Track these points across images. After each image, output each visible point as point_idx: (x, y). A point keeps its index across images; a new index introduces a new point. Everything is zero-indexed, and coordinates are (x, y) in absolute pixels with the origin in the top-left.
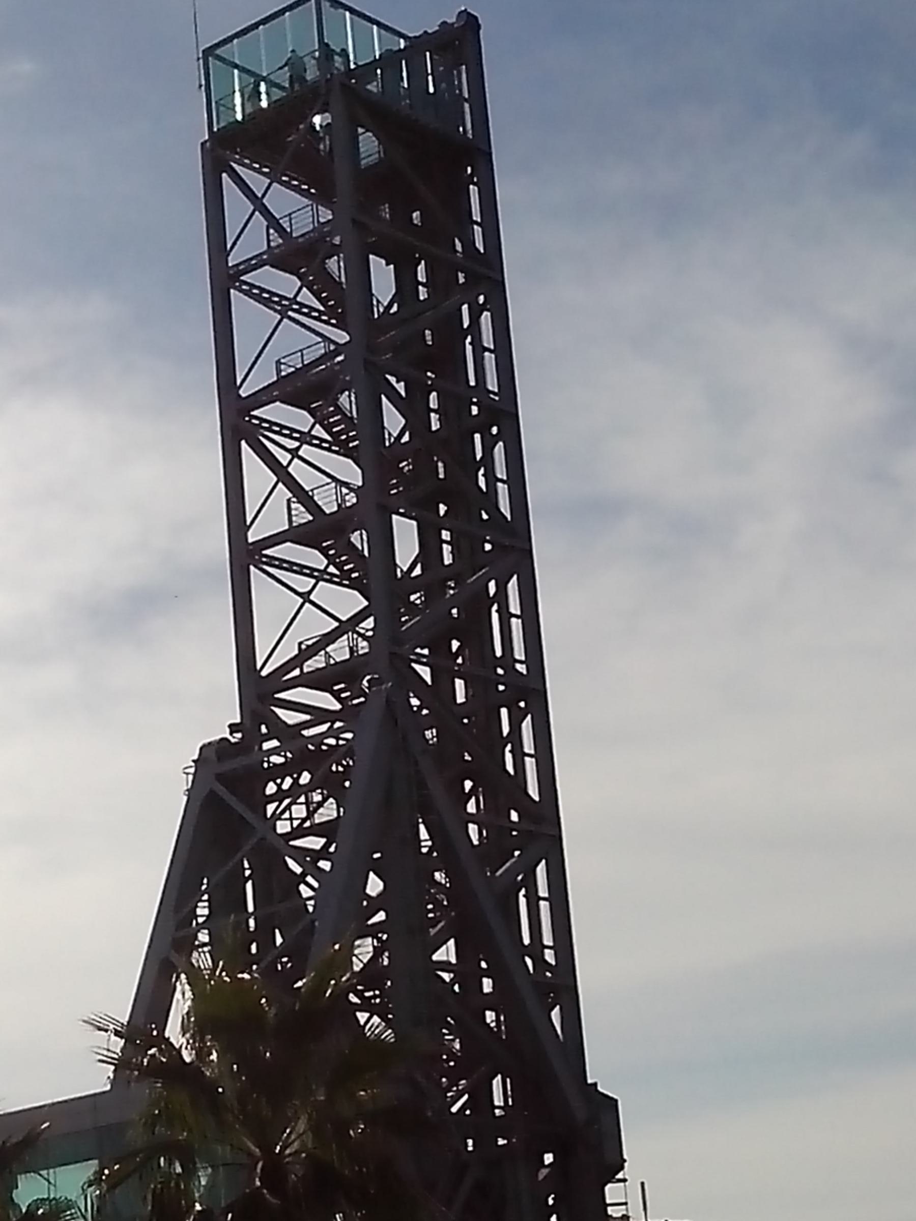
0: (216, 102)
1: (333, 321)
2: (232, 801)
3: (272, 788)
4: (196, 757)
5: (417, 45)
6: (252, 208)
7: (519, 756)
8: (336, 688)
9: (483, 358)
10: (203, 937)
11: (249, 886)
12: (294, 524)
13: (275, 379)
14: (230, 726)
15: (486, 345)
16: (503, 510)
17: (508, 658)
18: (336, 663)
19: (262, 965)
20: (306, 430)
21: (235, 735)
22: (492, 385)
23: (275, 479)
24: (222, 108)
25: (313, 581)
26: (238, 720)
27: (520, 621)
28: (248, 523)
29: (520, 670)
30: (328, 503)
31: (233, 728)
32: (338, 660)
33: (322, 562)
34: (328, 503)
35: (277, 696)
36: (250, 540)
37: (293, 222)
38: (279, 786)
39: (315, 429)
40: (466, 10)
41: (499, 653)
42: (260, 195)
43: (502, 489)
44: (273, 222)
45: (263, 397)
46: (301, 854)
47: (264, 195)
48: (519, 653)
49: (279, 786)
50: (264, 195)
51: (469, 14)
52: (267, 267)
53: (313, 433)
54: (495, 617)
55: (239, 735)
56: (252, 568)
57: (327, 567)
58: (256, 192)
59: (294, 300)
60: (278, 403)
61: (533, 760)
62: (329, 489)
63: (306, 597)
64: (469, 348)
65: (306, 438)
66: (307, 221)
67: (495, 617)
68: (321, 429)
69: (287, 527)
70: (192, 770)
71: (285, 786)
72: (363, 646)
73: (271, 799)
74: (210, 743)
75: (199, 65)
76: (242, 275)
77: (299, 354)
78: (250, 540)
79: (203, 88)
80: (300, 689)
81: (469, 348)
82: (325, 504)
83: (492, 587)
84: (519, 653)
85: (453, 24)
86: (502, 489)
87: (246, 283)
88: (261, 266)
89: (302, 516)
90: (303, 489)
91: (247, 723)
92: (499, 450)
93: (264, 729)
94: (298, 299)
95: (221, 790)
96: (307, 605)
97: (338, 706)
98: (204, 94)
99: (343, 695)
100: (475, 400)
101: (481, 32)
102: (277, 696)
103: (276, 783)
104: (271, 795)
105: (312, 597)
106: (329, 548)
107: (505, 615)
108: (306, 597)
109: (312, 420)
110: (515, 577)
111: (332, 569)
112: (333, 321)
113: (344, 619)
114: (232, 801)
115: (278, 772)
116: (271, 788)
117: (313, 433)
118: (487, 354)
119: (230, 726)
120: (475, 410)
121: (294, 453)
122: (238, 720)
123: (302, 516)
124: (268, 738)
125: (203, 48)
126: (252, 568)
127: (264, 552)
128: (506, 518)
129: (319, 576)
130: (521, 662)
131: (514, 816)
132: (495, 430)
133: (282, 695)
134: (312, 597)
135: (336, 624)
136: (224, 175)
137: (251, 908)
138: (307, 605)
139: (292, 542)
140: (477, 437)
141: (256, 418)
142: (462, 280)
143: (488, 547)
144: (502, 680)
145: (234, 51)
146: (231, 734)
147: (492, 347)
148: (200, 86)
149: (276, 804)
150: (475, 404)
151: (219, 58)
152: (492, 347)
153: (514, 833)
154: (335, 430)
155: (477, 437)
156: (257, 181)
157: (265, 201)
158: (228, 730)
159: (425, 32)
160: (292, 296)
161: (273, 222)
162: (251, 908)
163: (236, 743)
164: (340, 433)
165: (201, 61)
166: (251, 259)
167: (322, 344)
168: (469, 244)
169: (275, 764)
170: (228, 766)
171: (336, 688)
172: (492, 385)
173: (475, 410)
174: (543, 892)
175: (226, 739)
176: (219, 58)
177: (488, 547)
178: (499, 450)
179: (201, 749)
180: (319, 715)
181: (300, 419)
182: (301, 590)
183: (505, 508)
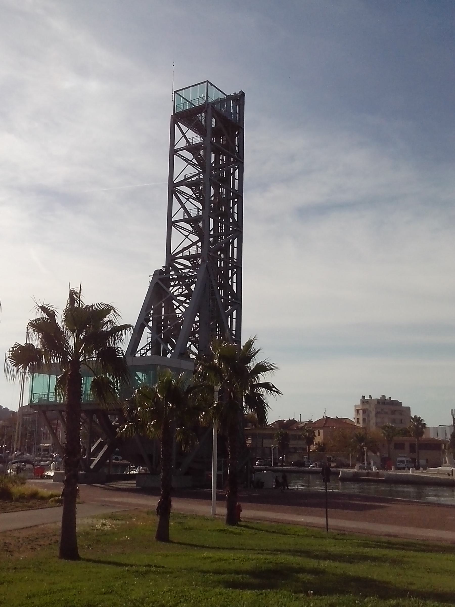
0: (176, 105)
1: (200, 167)
2: (162, 285)
3: (173, 283)
4: (153, 273)
5: (229, 98)
6: (181, 207)
7: (232, 282)
8: (190, 260)
9: (235, 181)
10: (151, 318)
11: (163, 309)
12: (185, 218)
13: (184, 179)
14: (163, 266)
15: (236, 178)
16: (235, 218)
17: (231, 329)
18: (192, 255)
19: (164, 331)
20: (191, 234)
21: (164, 269)
22: (236, 188)
23: (182, 136)
24: (177, 107)
25: (189, 233)
26: (165, 265)
27: (237, 214)
28: (175, 145)
29: (234, 333)
30: (194, 214)
31: (164, 267)
32: (192, 254)
33: (191, 193)
34: (194, 214)
35: (175, 260)
36: (173, 220)
37: (193, 140)
38: (175, 283)
39: (193, 160)
40: (242, 91)
41: (230, 256)
42: (185, 133)
43: (235, 285)
44: (186, 210)
45: (181, 183)
46: (179, 301)
47: (185, 203)
48: (235, 257)
49: (175, 283)
50: (185, 203)
51: (243, 92)
52: (185, 150)
53: (193, 196)
54: (231, 247)
55: (165, 269)
56: (172, 227)
57: (193, 194)
58: (184, 131)
59: (191, 161)
60: (184, 186)
61: (236, 249)
62: (195, 210)
63: (187, 236)
64: (232, 178)
65: (191, 197)
66: (194, 250)
67: (231, 247)
68: (195, 160)
69: (183, 218)
70: (152, 276)
71: (176, 283)
72: (199, 251)
73: (171, 286)
74: (158, 270)
75: (173, 95)
76: (178, 151)
77: (192, 139)
78: (173, 220)
79: (173, 101)
80: (182, 259)
81: (232, 178)
82: (194, 103)
83: (231, 240)
84: (235, 257)
85: (238, 94)
86: (235, 285)
87: (178, 154)
88: (184, 150)
89: (186, 217)
90: (187, 209)
91: (167, 266)
92: (235, 276)
93: (171, 269)
94: (192, 161)
95: (160, 282)
96: (187, 238)
97: (191, 266)
98: (173, 103)
99: (192, 262)
100: (231, 226)
101: (245, 97)
102: (175, 260)
103: (174, 282)
104: (172, 285)
105: (188, 237)
106: (192, 225)
107: (232, 318)
108: (187, 236)
109: (193, 157)
110: (236, 239)
111: (193, 231)
112: (200, 167)
113: (194, 241)
114: (162, 285)
115: (174, 280)
116: (172, 283)
117: (193, 196)
118: (236, 180)
119: (163, 266)
120: (231, 229)
121: (188, 200)
122: (165, 265)
123: (186, 217)
124: (171, 270)
125: (175, 91)
126: (172, 227)
127: (176, 224)
128: (236, 220)
129: (191, 232)
130: (235, 259)
131: (230, 297)
132: (236, 200)
133: (177, 260)
134: (188, 237)
135: (192, 243)
136: (176, 125)
137: (163, 314)
138: (187, 238)
139: (184, 222)
140: (231, 201)
141: (177, 189)
142: (231, 195)
143: (230, 265)
144: (230, 300)
145: (183, 93)
146: (163, 268)
147: (237, 179)
148: (172, 101)
149: (173, 287)
150: (232, 192)
151: (178, 94)
152: (237, 179)
153: (229, 302)
154: (197, 195)
155: (231, 201)
156: (184, 129)
157: (185, 205)
158: (162, 267)
159: (230, 95)
160: (191, 160)
161: (186, 210)
162: (163, 314)
163: (164, 271)
164: (198, 196)
165: (173, 94)
166: (182, 148)
167: (198, 137)
168: (234, 219)
169: (174, 278)
170: (162, 276)
171: (190, 260)
172: (236, 188)
173: (231, 229)
174: (235, 246)
175: (161, 270)
176: (178, 94)
177: (230, 265)
178: (235, 276)
179: (155, 271)
180: (186, 267)
181: (189, 191)
182: (185, 235)
183: (235, 289)
